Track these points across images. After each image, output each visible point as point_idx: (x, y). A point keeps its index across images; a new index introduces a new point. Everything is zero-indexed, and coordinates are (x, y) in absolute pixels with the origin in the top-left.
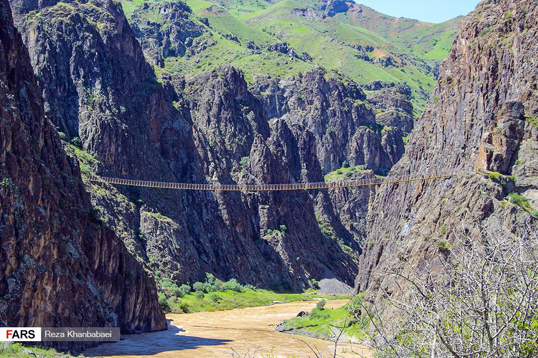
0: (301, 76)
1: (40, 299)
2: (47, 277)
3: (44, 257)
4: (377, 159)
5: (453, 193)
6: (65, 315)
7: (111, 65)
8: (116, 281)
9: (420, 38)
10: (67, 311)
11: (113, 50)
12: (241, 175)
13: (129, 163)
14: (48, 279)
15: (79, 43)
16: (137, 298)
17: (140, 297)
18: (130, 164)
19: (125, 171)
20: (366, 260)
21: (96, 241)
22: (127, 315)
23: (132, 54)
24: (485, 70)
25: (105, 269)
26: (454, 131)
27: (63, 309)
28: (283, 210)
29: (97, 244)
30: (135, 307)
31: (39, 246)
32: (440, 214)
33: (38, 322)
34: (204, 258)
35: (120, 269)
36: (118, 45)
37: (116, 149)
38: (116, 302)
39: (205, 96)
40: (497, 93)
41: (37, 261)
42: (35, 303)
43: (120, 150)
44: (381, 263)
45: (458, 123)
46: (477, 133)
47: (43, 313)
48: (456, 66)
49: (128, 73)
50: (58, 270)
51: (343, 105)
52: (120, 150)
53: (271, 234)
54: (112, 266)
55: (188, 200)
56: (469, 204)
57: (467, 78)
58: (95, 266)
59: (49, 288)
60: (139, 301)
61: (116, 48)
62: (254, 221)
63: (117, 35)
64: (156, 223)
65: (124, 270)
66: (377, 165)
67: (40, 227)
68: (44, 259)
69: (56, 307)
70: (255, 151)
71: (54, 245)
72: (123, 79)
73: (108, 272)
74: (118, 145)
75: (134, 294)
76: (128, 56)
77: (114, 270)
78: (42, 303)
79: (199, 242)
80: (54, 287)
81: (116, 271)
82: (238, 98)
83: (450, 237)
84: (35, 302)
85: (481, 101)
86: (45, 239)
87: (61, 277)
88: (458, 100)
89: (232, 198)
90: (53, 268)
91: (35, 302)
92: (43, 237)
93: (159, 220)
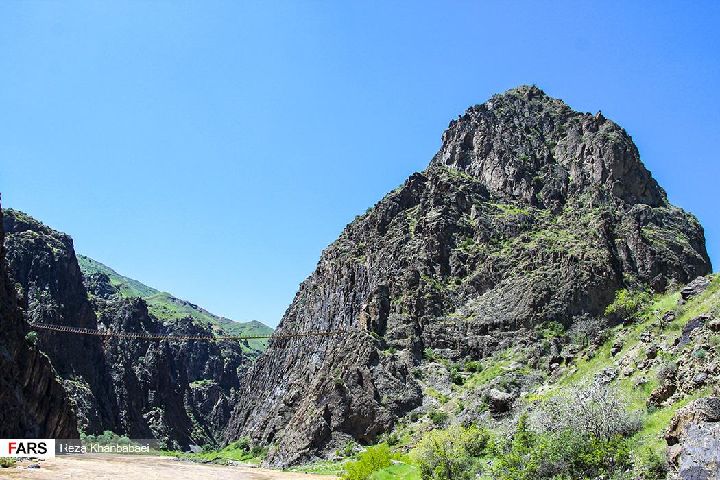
0: (177, 320)
4: (221, 377)
5: (344, 344)
12: (137, 368)
16: (59, 421)
18: (60, 345)
19: (57, 349)
20: (235, 422)
23: (74, 274)
24: (345, 277)
28: (164, 395)
30: (56, 428)
32: (333, 360)
34: (107, 420)
35: (48, 392)
36: (66, 265)
39: (119, 314)
40: (355, 293)
45: (323, 314)
46: (339, 319)
49: (70, 285)
53: (155, 410)
55: (99, 378)
56: (358, 351)
57: (331, 284)
61: (64, 265)
62: (143, 400)
64: (75, 388)
65: (51, 393)
66: (220, 381)
70: (149, 353)
76: (71, 275)
79: (104, 408)
81: (44, 393)
83: (344, 376)
85: (343, 298)
88: (323, 298)
89: (129, 376)
93: (77, 386)
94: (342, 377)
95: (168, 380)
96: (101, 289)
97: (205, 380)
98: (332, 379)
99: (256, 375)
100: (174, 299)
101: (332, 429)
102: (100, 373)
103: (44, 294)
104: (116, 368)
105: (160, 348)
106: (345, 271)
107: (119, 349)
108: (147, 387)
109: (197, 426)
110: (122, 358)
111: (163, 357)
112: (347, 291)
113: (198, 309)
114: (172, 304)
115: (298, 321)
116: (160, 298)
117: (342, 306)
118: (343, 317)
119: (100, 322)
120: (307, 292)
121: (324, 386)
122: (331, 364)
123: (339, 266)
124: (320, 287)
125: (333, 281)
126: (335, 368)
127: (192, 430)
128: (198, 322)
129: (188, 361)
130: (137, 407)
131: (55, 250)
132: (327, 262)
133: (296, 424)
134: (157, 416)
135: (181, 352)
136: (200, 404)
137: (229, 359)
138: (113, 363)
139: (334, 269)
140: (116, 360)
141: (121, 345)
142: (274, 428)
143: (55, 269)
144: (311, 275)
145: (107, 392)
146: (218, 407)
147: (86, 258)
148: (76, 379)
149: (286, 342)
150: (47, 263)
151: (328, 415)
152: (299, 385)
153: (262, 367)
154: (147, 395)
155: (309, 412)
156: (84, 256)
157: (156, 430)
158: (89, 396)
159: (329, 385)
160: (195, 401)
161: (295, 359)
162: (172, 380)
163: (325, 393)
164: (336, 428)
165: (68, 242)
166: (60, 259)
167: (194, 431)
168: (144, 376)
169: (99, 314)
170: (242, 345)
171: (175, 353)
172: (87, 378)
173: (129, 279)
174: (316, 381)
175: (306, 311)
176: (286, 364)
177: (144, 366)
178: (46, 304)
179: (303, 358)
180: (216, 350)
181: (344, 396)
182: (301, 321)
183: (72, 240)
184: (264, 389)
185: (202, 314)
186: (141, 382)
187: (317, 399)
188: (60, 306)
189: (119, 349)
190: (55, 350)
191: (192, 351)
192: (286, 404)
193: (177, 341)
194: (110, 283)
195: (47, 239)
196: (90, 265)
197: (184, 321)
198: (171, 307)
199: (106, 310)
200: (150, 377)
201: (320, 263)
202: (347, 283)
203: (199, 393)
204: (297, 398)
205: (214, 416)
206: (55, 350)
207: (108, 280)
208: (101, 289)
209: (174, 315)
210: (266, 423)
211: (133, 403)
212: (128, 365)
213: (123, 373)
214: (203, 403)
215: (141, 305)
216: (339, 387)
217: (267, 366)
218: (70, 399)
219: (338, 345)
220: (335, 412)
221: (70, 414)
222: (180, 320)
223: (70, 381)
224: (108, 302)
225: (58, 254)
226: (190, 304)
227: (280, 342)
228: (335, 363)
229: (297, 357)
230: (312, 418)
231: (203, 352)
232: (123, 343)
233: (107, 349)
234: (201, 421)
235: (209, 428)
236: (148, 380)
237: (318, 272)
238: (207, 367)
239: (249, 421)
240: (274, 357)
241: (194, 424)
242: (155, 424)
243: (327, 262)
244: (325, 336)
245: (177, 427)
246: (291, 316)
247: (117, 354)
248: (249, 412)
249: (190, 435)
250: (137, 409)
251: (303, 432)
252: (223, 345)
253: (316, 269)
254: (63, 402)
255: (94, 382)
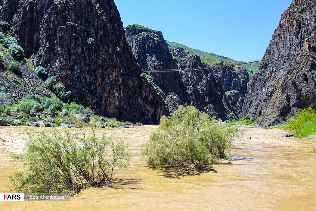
0: (216, 64)
1: (112, 98)
2: (116, 89)
3: (115, 80)
4: (239, 88)
5: (295, 61)
6: (125, 107)
7: (158, 50)
8: (152, 103)
9: (245, 66)
10: (125, 106)
11: (159, 46)
12: (199, 87)
13: (163, 79)
14: (117, 90)
15: (148, 43)
16: (161, 111)
17: (162, 110)
20: (245, 107)
21: (144, 86)
22: (156, 117)
23: (165, 48)
24: (295, 26)
25: (148, 98)
26: (283, 51)
27: (123, 105)
28: (212, 98)
29: (144, 87)
31: (113, 75)
32: (290, 70)
33: (111, 108)
35: (154, 99)
36: (161, 45)
37: (159, 75)
38: (152, 112)
41: (112, 81)
42: (109, 100)
43: (160, 75)
44: (251, 106)
45: (284, 48)
46: (294, 49)
47: (114, 105)
48: (282, 29)
50: (122, 87)
51: (229, 72)
52: (160, 75)
53: (209, 105)
54: (150, 97)
55: (182, 93)
57: (287, 31)
58: (143, 96)
59: (117, 94)
60: (161, 112)
61: (160, 45)
62: (203, 101)
63: (160, 42)
64: (172, 98)
67: (114, 67)
68: (114, 81)
69: (120, 103)
70: (204, 79)
71: (120, 76)
72: (162, 54)
73: (149, 99)
74: (160, 74)
75: (159, 109)
76: (164, 49)
77: (151, 99)
78: (113, 100)
80: (120, 94)
81: (152, 99)
82: (198, 64)
84: (110, 99)
85: (294, 38)
86: (116, 73)
87: (123, 90)
88: (284, 40)
89: (195, 91)
90: (120, 86)
91: (110, 99)
92: (114, 71)
93: (173, 97)
94: (295, 78)
95: (213, 91)
96: (181, 55)
97: (232, 90)
98: (289, 80)
99: (253, 84)
100: (215, 55)
101: (291, 106)
102: (182, 91)
103: (153, 59)
104: (189, 88)
105: (208, 77)
106: (295, 23)
107: (189, 79)
108: (204, 95)
109: (230, 111)
110: (191, 83)
111: (210, 81)
112: (297, 34)
113: (228, 59)
114: (214, 57)
115: (272, 54)
116: (209, 55)
117: (295, 42)
118: (295, 48)
119: (179, 68)
120: (275, 38)
121: (286, 84)
122: (289, 72)
123: (291, 21)
124: (282, 34)
125: (288, 29)
126: (291, 74)
127: (227, 114)
128: (226, 64)
129: (223, 82)
130: (200, 104)
131: (155, 39)
132: (284, 20)
133: (272, 104)
134: (210, 108)
135: (219, 78)
136: (231, 102)
137: (243, 79)
138: (187, 86)
139: (289, 23)
140: (189, 84)
141: (190, 77)
142: (262, 108)
143: (156, 47)
144: (276, 28)
145: (187, 99)
146: (239, 102)
147: (174, 43)
148: (172, 94)
149: (267, 66)
150: (153, 45)
151: (288, 99)
152: (274, 85)
153: (256, 80)
154: (204, 99)
155: (279, 98)
156: (173, 42)
157: (210, 114)
158: (178, 101)
159: (288, 83)
160: (228, 100)
161: (271, 73)
162: (216, 91)
163: (286, 88)
164: (293, 106)
165: (160, 34)
166: (158, 42)
167: (228, 114)
168: (203, 90)
169: (179, 65)
170: (249, 73)
171: (216, 79)
172: (177, 93)
173: (194, 49)
174: (281, 82)
175: (275, 48)
176: (267, 76)
177: (202, 86)
178: (155, 63)
179: (275, 72)
180: (236, 76)
181: (297, 88)
182: (273, 53)
183: (162, 33)
184: (258, 90)
185: (230, 61)
186: (201, 93)
187: (282, 91)
188: (161, 63)
189: (189, 79)
190: (162, 83)
191: (224, 77)
192: (267, 96)
193: (217, 74)
194: (184, 52)
195: (151, 35)
196: (176, 45)
197: (219, 64)
198: (213, 58)
199: (182, 63)
200: (205, 90)
201: (280, 21)
202: (296, 29)
203: (230, 97)
204: (272, 93)
205: (238, 107)
206: (162, 83)
207: (183, 50)
208: (181, 55)
209: (214, 62)
210: (257, 106)
211: (198, 103)
212: (194, 86)
213: (193, 90)
214: (232, 102)
215: (197, 58)
216: (294, 83)
217: (258, 79)
218: (165, 101)
219: (292, 61)
220: (292, 97)
221: (165, 108)
222: (217, 64)
223: (169, 95)
224: (183, 59)
225: (157, 41)
226: (223, 57)
227: (264, 66)
228: (291, 71)
229: (272, 72)
230: (280, 101)
231: (230, 78)
232: (191, 76)
233: (184, 80)
234: (232, 109)
235: (236, 112)
236: (205, 92)
237: (280, 26)
238: (233, 84)
239: (251, 106)
240: (261, 74)
241: (228, 110)
242: (209, 112)
243: (284, 20)
244: (286, 59)
245: (220, 112)
246: (268, 52)
247: (189, 82)
248: (251, 102)
249: (226, 116)
250: (201, 106)
251: (275, 109)
252: (239, 73)
253: (278, 25)
254: (161, 103)
255: (180, 95)
